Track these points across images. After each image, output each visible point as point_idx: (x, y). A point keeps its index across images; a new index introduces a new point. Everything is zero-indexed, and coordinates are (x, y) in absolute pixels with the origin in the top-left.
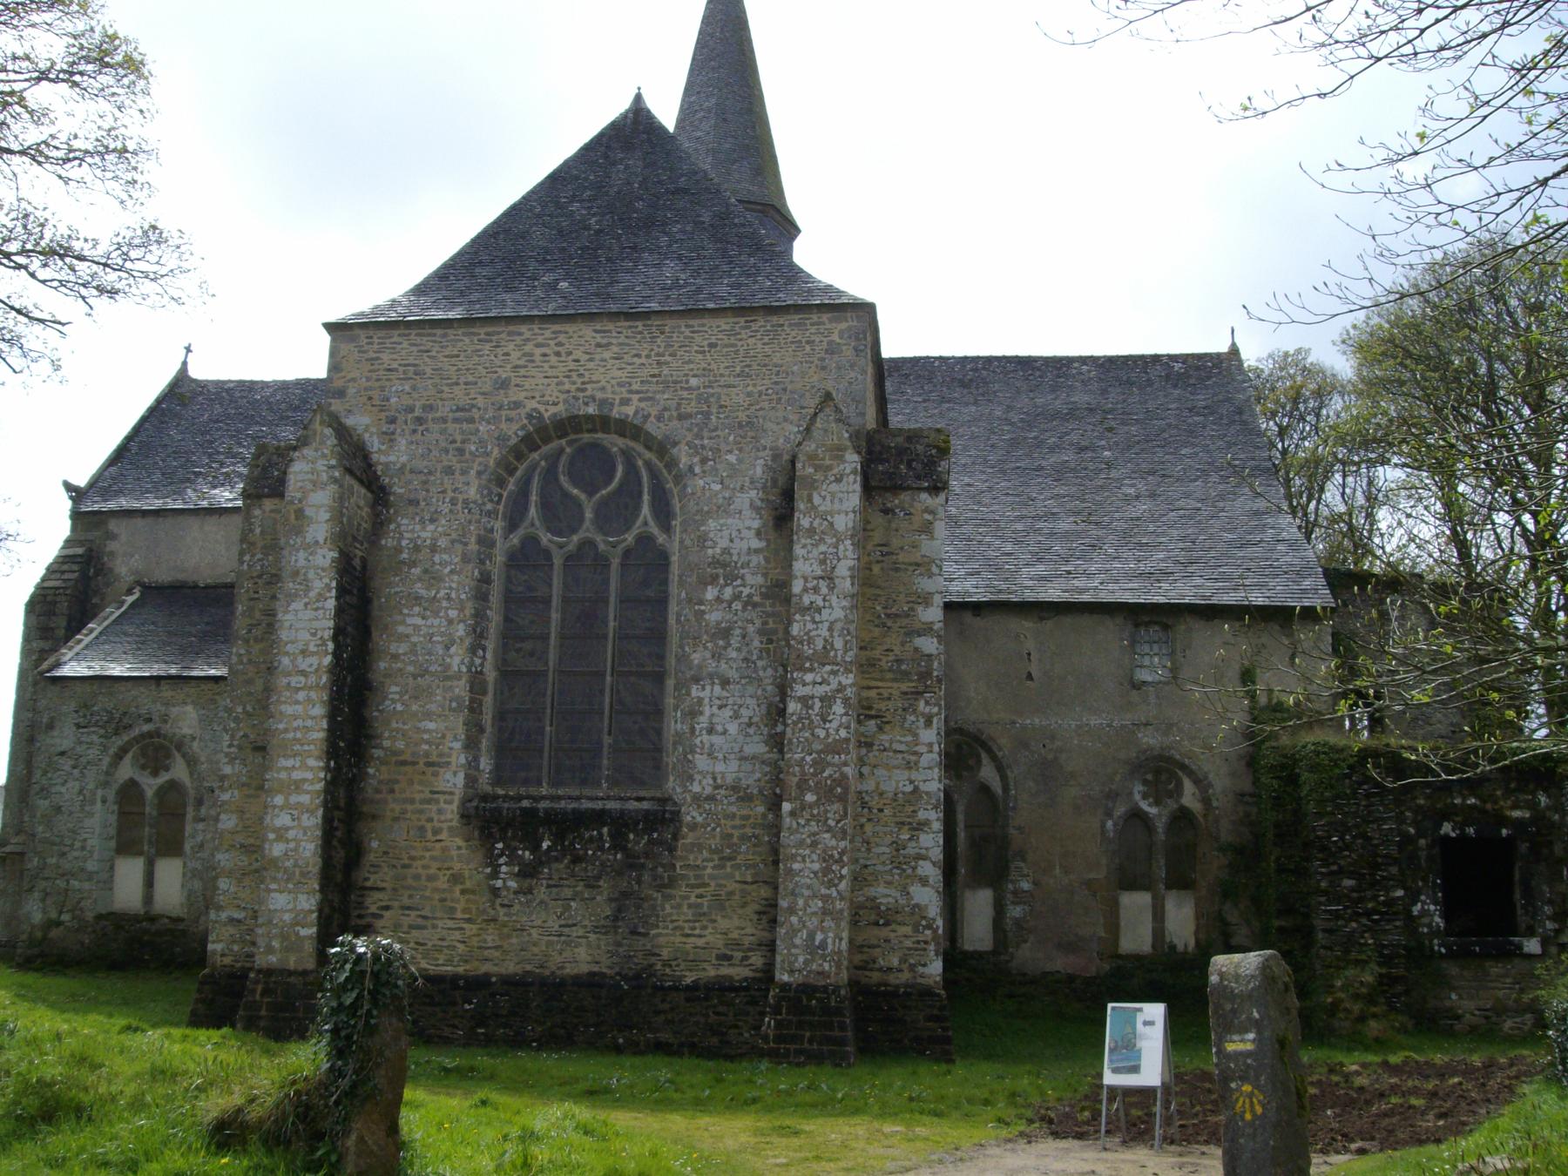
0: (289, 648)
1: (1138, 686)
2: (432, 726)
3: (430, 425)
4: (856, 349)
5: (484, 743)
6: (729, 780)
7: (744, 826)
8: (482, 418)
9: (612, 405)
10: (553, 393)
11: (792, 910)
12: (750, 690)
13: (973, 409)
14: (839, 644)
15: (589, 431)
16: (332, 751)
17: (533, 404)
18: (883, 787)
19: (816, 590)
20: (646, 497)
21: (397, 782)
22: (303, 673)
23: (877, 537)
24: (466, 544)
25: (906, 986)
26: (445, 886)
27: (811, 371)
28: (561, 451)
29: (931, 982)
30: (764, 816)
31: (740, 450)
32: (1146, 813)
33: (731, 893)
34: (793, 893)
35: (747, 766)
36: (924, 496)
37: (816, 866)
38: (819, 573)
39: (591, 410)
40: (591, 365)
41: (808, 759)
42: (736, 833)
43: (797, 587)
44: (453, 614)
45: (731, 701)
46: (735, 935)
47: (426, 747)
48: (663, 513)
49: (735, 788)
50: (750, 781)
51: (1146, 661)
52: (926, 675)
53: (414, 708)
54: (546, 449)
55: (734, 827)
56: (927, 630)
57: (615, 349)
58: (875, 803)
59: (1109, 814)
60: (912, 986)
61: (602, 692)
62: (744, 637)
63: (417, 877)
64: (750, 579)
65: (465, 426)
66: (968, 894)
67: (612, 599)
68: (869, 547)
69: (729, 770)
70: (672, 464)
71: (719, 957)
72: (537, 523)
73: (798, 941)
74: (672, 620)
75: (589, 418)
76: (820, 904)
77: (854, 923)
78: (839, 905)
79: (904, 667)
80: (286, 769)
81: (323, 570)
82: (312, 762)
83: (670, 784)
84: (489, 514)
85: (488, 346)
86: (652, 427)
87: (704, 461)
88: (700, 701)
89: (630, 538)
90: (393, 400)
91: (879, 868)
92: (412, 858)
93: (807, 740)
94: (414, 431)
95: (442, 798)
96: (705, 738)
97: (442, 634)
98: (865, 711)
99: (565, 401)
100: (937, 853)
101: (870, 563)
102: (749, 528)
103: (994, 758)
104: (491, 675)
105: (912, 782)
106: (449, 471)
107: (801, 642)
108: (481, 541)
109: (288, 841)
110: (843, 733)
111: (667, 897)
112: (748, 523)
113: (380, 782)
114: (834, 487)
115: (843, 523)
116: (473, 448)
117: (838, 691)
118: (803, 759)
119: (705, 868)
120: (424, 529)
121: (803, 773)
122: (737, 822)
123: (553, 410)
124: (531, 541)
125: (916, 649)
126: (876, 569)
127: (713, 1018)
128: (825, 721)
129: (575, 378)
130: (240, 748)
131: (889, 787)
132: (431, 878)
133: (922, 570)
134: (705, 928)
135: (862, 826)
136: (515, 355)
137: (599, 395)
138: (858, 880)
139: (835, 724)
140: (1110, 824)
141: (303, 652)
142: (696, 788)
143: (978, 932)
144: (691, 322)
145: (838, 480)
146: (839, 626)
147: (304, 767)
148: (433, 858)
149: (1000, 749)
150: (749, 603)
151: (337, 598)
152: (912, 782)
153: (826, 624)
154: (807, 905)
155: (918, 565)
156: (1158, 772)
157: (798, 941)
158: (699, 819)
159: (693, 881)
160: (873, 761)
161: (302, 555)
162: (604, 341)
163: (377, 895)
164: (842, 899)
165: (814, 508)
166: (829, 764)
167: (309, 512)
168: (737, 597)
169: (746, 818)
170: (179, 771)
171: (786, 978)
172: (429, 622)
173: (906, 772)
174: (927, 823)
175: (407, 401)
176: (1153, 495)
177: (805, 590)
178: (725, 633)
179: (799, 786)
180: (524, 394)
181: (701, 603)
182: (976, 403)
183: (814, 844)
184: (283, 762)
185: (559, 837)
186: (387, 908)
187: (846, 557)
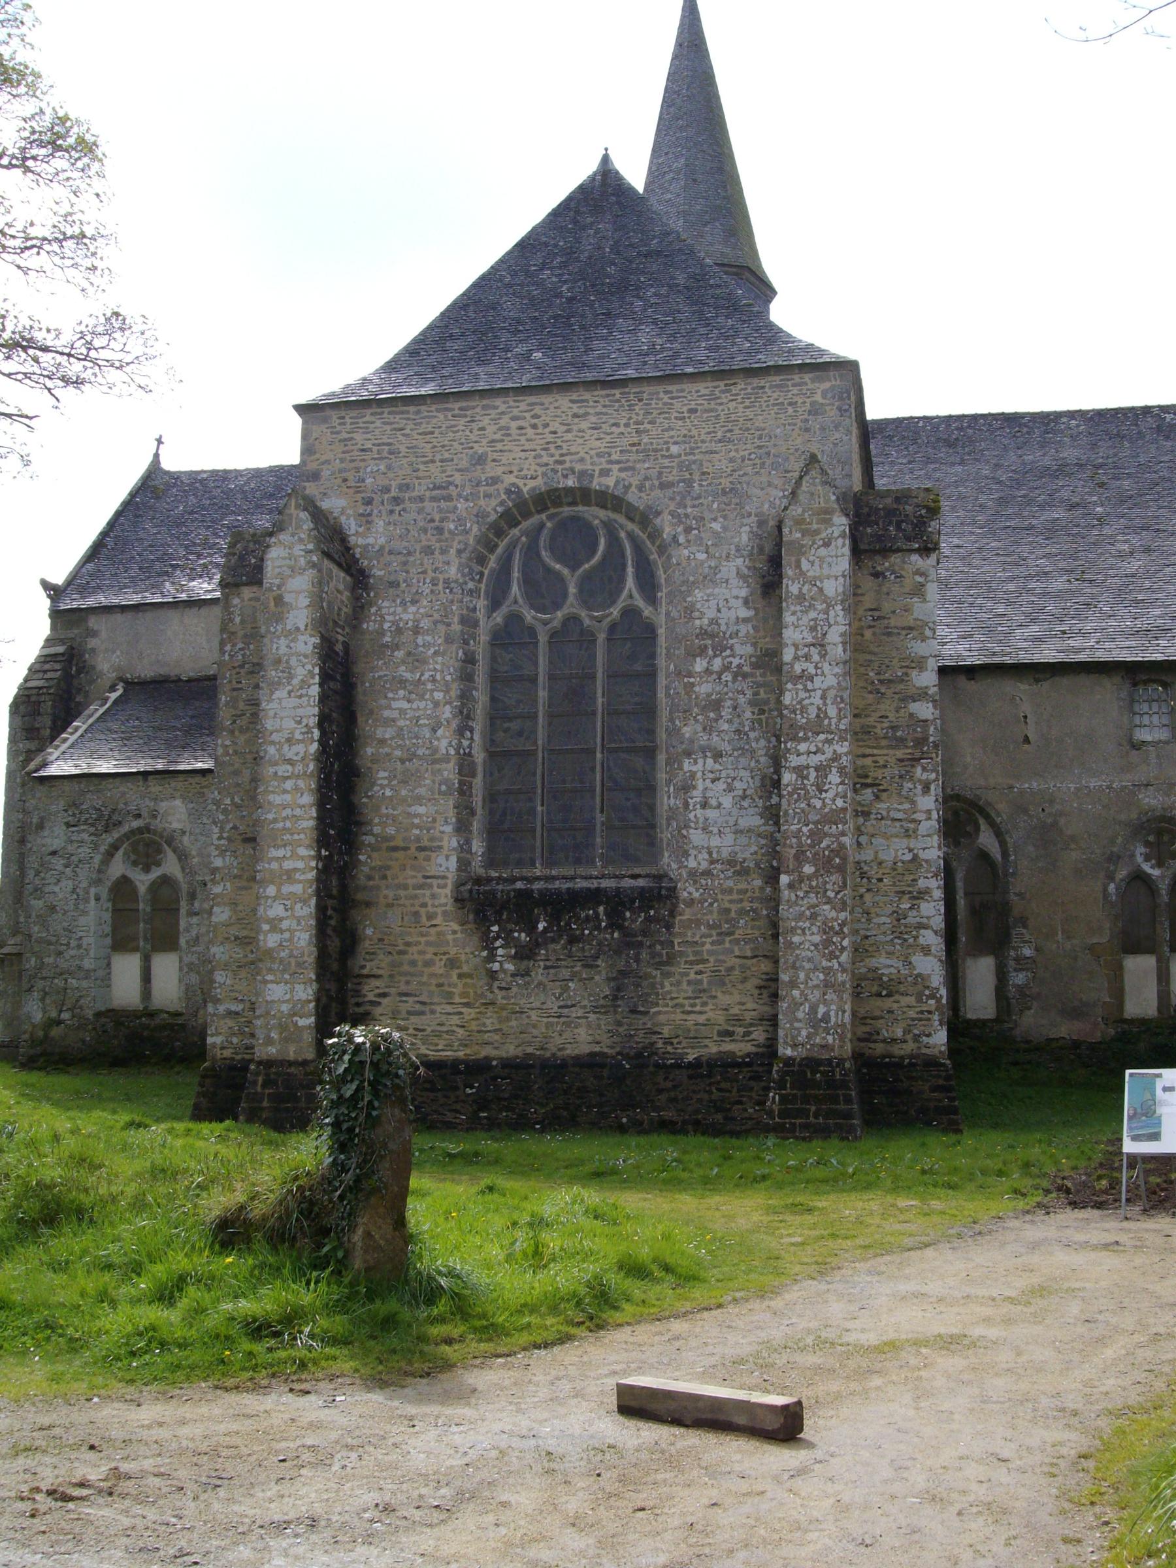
0: (275, 737)
1: (1137, 746)
2: (422, 810)
3: (408, 505)
4: (839, 409)
5: (476, 826)
6: (725, 854)
7: (741, 901)
8: (460, 496)
9: (592, 476)
10: (530, 467)
11: (793, 984)
12: (743, 761)
13: (959, 468)
14: (832, 712)
15: (570, 504)
16: (322, 840)
17: (511, 479)
18: (881, 856)
19: (807, 657)
20: (630, 570)
21: (388, 868)
22: (290, 762)
23: (868, 601)
24: (449, 625)
25: (911, 1056)
26: (441, 971)
27: (795, 434)
28: (542, 526)
29: (936, 1051)
30: (762, 889)
31: (725, 517)
32: (1149, 875)
33: (732, 968)
34: (794, 967)
35: (743, 840)
36: (915, 557)
37: (817, 939)
38: (810, 640)
39: (570, 482)
40: (569, 436)
41: (805, 829)
42: (734, 907)
43: (788, 655)
44: (439, 696)
45: (724, 774)
46: (735, 1010)
47: (417, 832)
48: (648, 585)
49: (731, 863)
50: (747, 855)
51: (1146, 720)
52: (921, 741)
53: (404, 792)
54: (525, 524)
55: (731, 902)
56: (922, 695)
57: (593, 419)
58: (873, 872)
59: (1111, 878)
60: (917, 1056)
61: (593, 769)
62: (735, 708)
63: (413, 963)
64: (739, 649)
65: (443, 504)
66: (969, 962)
67: (599, 675)
68: (861, 612)
69: (724, 844)
70: (655, 535)
71: (720, 1034)
72: (520, 601)
73: (800, 1015)
74: (661, 694)
75: (569, 491)
76: (822, 976)
77: (857, 995)
78: (841, 977)
79: (899, 734)
80: (277, 859)
81: (306, 656)
82: (303, 851)
83: (666, 860)
84: (471, 592)
85: (463, 421)
86: (632, 497)
87: (688, 530)
88: (693, 775)
89: (615, 612)
90: (369, 481)
91: (881, 938)
92: (408, 944)
93: (803, 811)
94: (392, 512)
95: (435, 882)
96: (699, 812)
97: (429, 717)
98: (861, 780)
99: (544, 474)
100: (938, 922)
101: (862, 628)
102: (737, 597)
103: (992, 824)
104: (479, 756)
105: (910, 850)
106: (428, 551)
107: (794, 712)
108: (463, 621)
109: (282, 931)
110: (840, 803)
111: (667, 975)
112: (735, 592)
113: (372, 869)
114: (823, 552)
115: (833, 588)
116: (452, 526)
117: (834, 760)
118: (800, 830)
119: (703, 944)
120: (405, 611)
121: (800, 845)
122: (735, 897)
123: (531, 484)
124: (514, 618)
125: (911, 715)
126: (868, 634)
127: (716, 1095)
128: (821, 791)
129: (553, 450)
130: (229, 840)
131: (888, 856)
132: (427, 964)
133: (915, 633)
134: (704, 1004)
135: (861, 896)
136: (491, 429)
137: (578, 467)
138: (859, 951)
139: (830, 794)
140: (1112, 887)
141: (289, 740)
142: (692, 863)
143: (980, 1001)
144: (670, 388)
145: (827, 544)
146: (831, 694)
147: (295, 856)
148: (428, 943)
149: (998, 815)
150: (739, 674)
151: (321, 685)
152: (910, 850)
153: (819, 693)
154: (808, 977)
155: (911, 628)
156: (1159, 833)
157: (800, 1015)
158: (696, 895)
159: (691, 958)
160: (871, 830)
161: (283, 642)
162: (582, 411)
163: (375, 983)
164: (844, 971)
165: (802, 573)
166: (826, 835)
167: (288, 598)
168: (726, 668)
169: (746, 891)
170: (170, 866)
171: (789, 1052)
172: (415, 706)
173: (905, 840)
174: (927, 891)
175: (382, 481)
176: (1148, 550)
177: (796, 658)
178: (716, 705)
179: (796, 857)
180: (502, 469)
181: (690, 675)
182: (962, 462)
183: (814, 916)
184: (274, 853)
185: (554, 918)
186: (384, 995)
187: (836, 623)
